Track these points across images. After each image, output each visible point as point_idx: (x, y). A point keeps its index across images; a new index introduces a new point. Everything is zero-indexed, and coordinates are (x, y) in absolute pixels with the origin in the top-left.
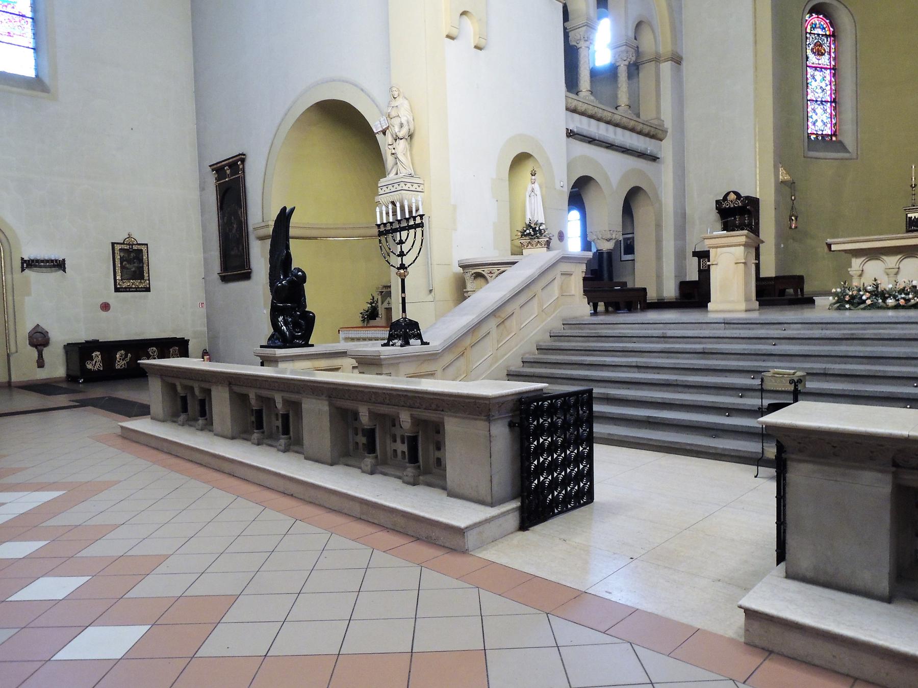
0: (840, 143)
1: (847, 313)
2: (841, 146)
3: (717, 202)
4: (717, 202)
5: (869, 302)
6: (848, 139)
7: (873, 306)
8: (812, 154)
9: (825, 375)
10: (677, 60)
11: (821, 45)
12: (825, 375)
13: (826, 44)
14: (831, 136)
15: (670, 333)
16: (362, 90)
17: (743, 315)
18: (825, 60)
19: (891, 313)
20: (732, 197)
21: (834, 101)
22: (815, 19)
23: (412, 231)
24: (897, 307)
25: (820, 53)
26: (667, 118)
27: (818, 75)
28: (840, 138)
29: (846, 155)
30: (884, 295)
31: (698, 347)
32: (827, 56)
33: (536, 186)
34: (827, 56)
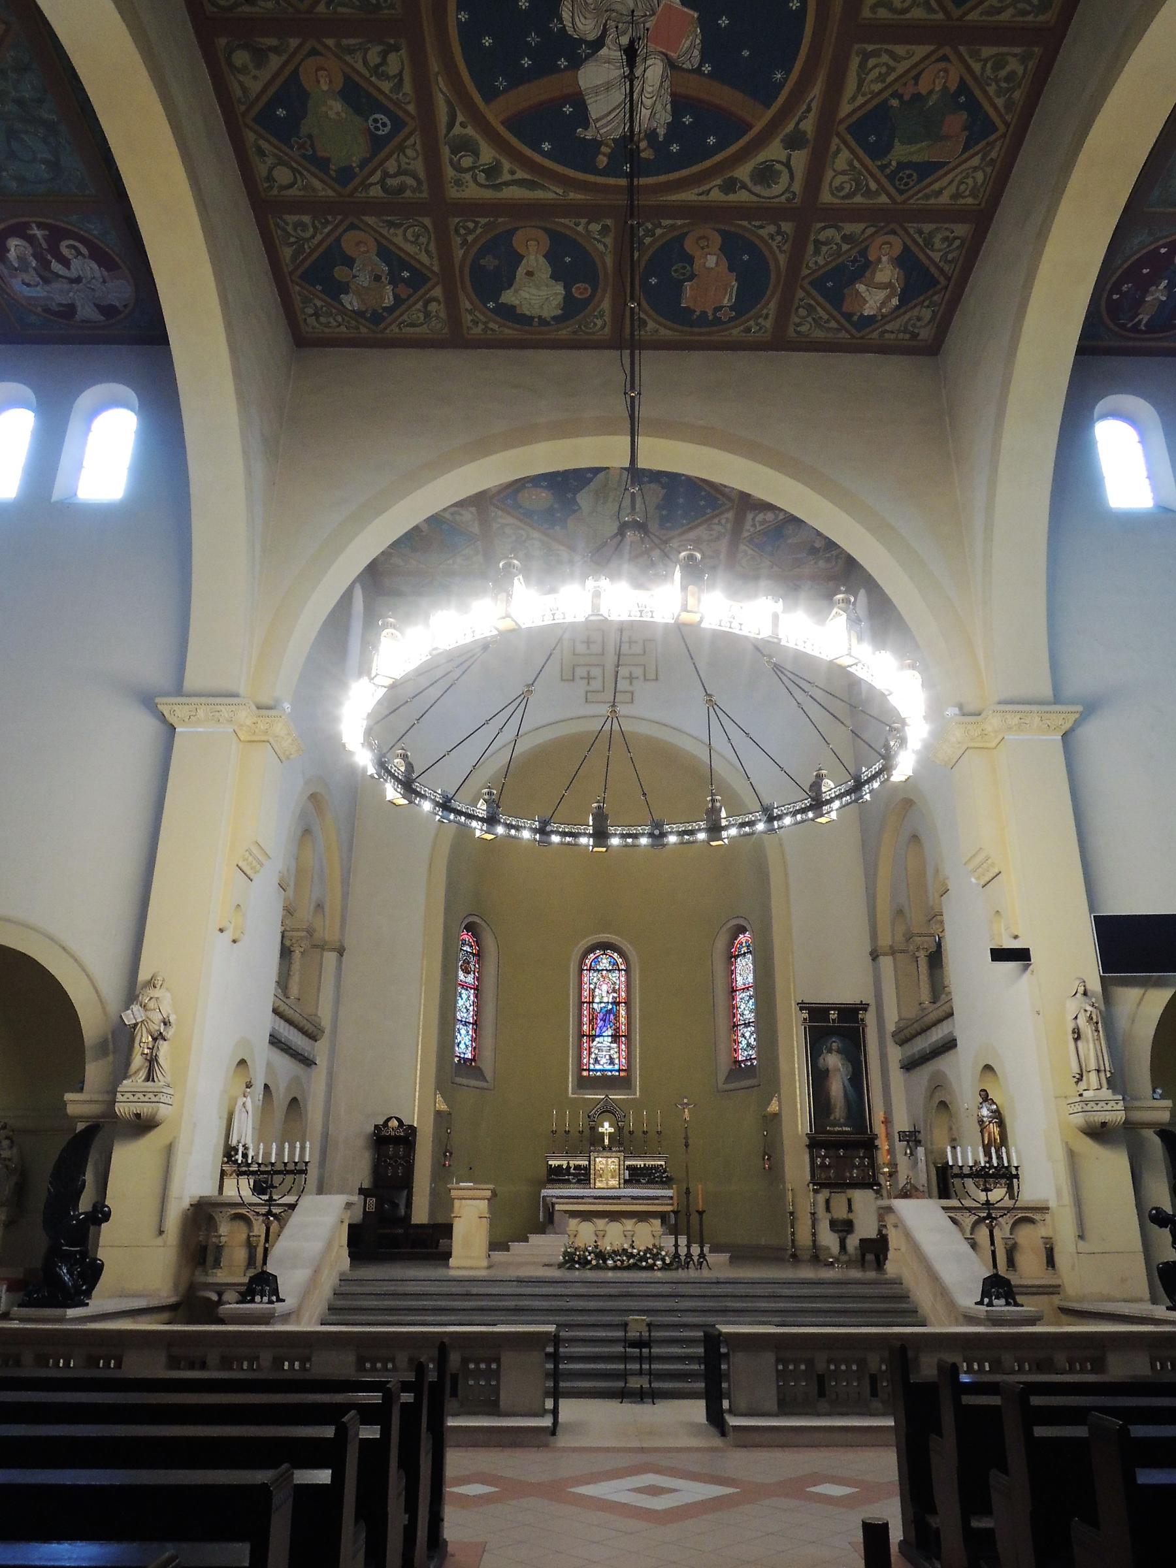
0: (479, 1069)
1: (577, 1273)
2: (478, 1073)
3: (376, 1127)
4: (376, 1127)
5: (594, 1262)
6: (487, 1066)
7: (597, 1267)
8: (459, 1080)
9: (597, 1325)
10: (341, 951)
11: (469, 963)
12: (597, 1325)
13: (472, 960)
14: (471, 1060)
15: (474, 1290)
16: (64, 949)
17: (482, 1273)
18: (470, 979)
19: (610, 1274)
20: (395, 1123)
21: (475, 1023)
22: (467, 937)
23: (290, 1178)
24: (615, 1268)
25: (467, 972)
26: (325, 1018)
27: (464, 993)
28: (479, 1064)
29: (484, 1085)
30: (601, 1255)
31: (511, 1304)
32: (472, 975)
33: (249, 1101)
34: (472, 975)
